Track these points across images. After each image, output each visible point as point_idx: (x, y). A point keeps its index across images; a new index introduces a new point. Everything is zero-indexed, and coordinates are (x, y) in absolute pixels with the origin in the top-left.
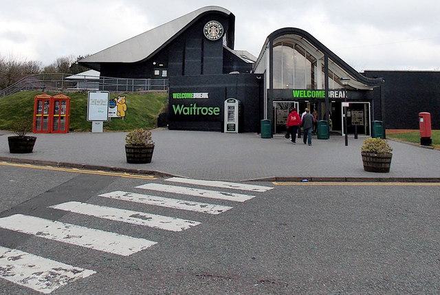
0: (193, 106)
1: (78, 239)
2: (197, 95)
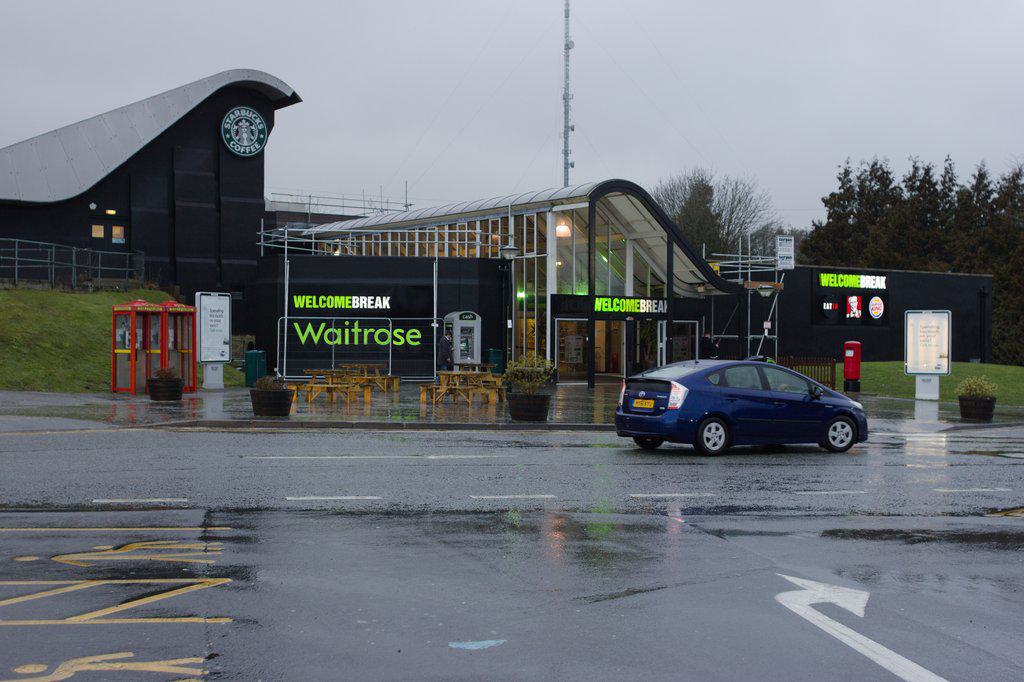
0: (351, 326)
2: (361, 302)
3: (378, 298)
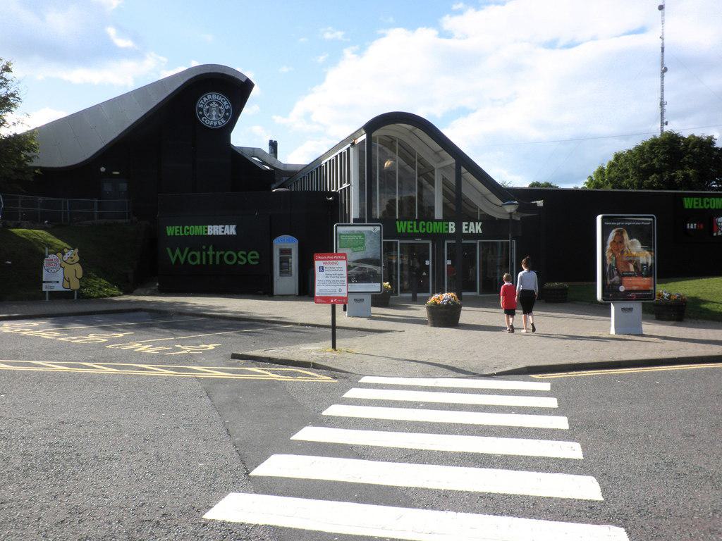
0: (207, 249)
1: (78, 272)
2: (214, 230)
3: (472, 224)
